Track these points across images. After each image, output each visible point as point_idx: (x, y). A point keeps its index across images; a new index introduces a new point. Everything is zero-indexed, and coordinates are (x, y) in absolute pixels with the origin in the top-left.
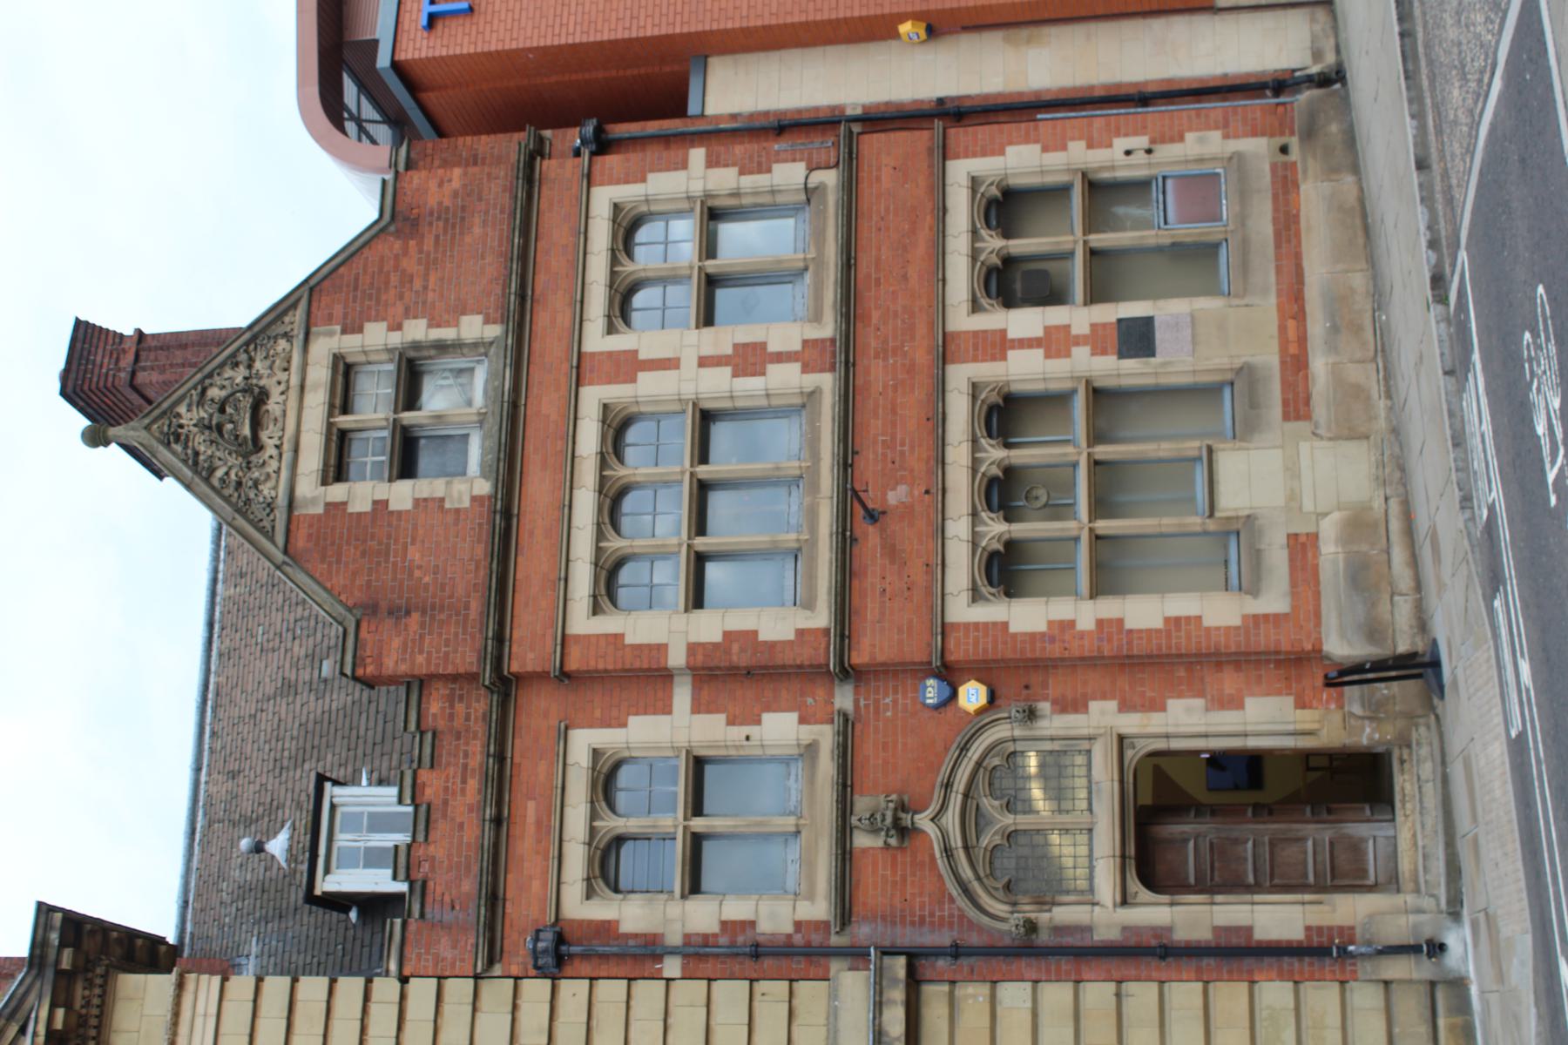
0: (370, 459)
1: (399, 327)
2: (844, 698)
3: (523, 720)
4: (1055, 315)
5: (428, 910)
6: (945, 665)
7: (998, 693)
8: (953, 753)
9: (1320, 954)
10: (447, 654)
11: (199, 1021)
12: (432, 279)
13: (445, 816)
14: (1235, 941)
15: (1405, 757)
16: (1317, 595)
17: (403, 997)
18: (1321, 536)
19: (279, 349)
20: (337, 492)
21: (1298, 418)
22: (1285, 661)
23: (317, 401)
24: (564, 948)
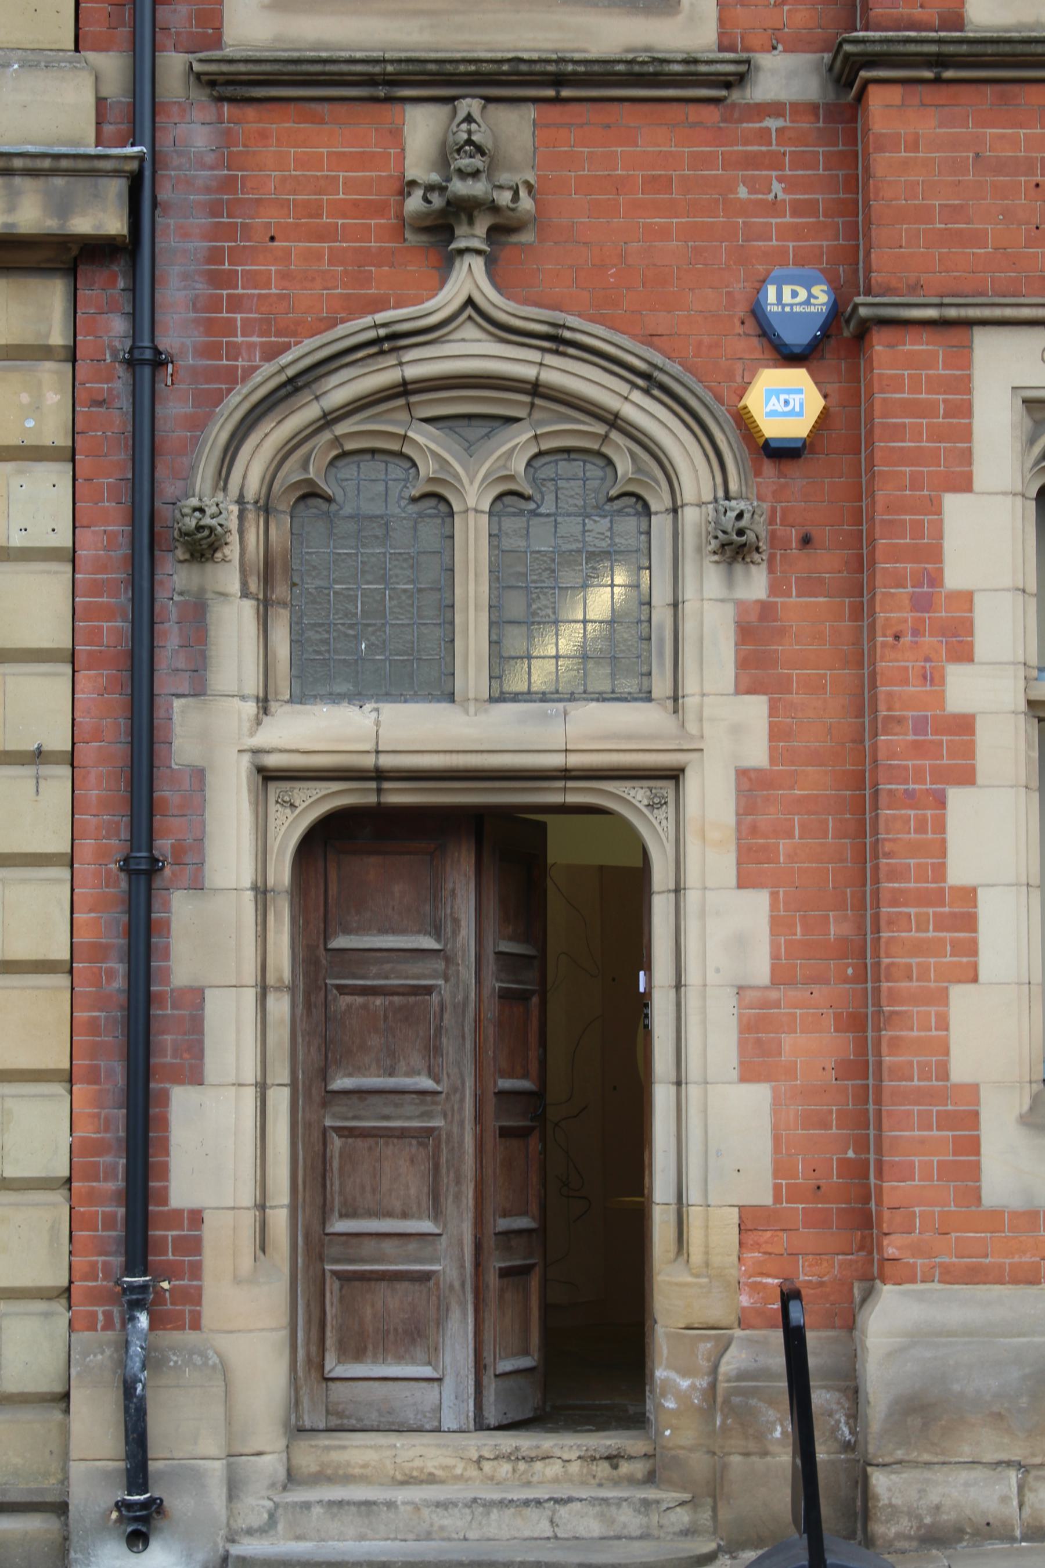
2: (785, 77)
6: (864, 330)
7: (794, 470)
8: (638, 353)
9: (135, 1247)
14: (167, 1043)
15: (625, 1468)
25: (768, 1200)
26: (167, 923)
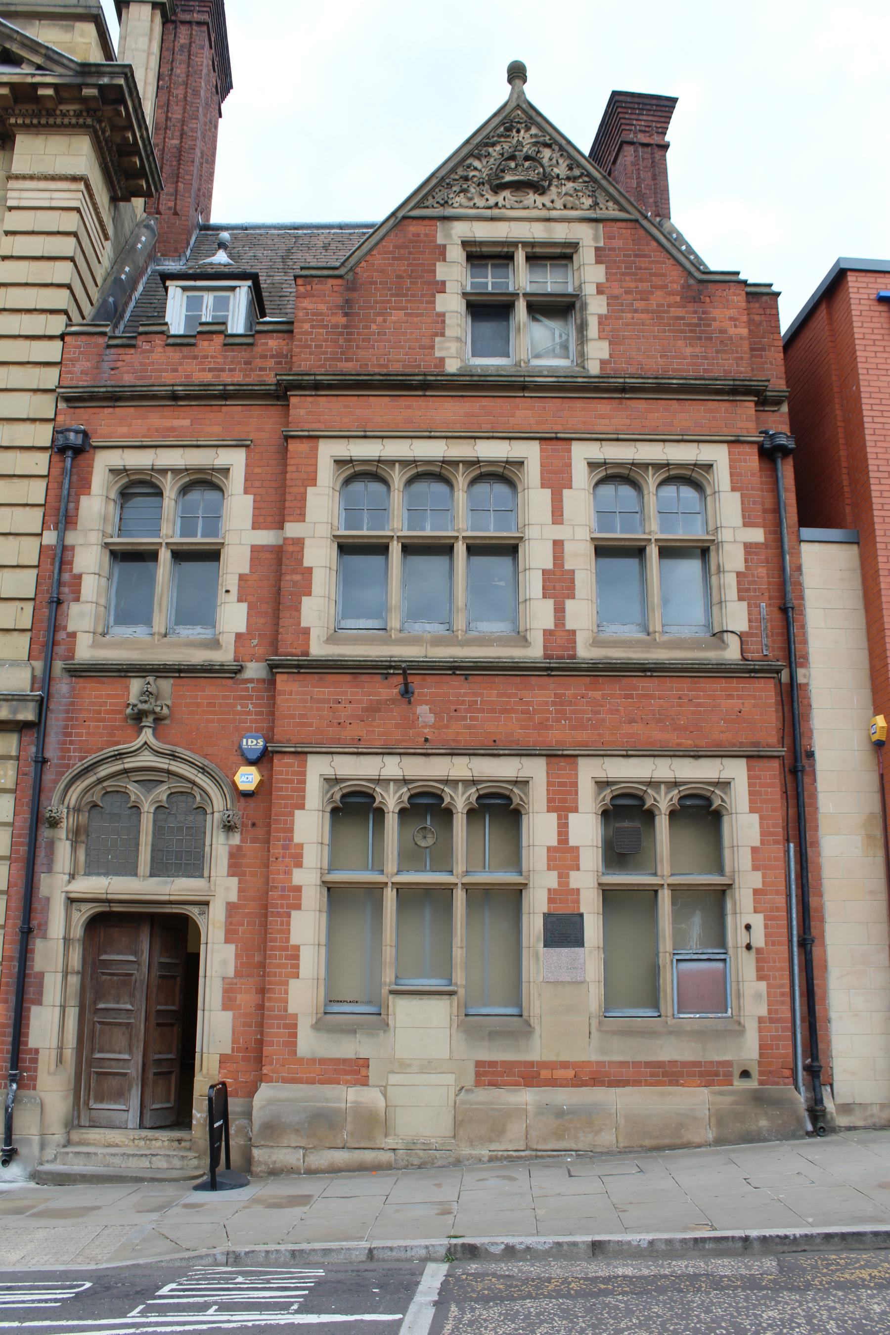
0: (490, 280)
1: (600, 291)
2: (254, 670)
3: (256, 412)
4: (591, 858)
5: (113, 351)
7: (249, 799)
10: (310, 347)
11: (47, 195)
12: (643, 316)
13: (184, 357)
14: (31, 990)
15: (183, 1144)
16: (312, 1082)
17: (51, 338)
18: (366, 1088)
19: (583, 200)
20: (456, 254)
21: (478, 1074)
22: (256, 1053)
23: (537, 232)
24: (70, 453)
25: (229, 1052)
26: (34, 950)
